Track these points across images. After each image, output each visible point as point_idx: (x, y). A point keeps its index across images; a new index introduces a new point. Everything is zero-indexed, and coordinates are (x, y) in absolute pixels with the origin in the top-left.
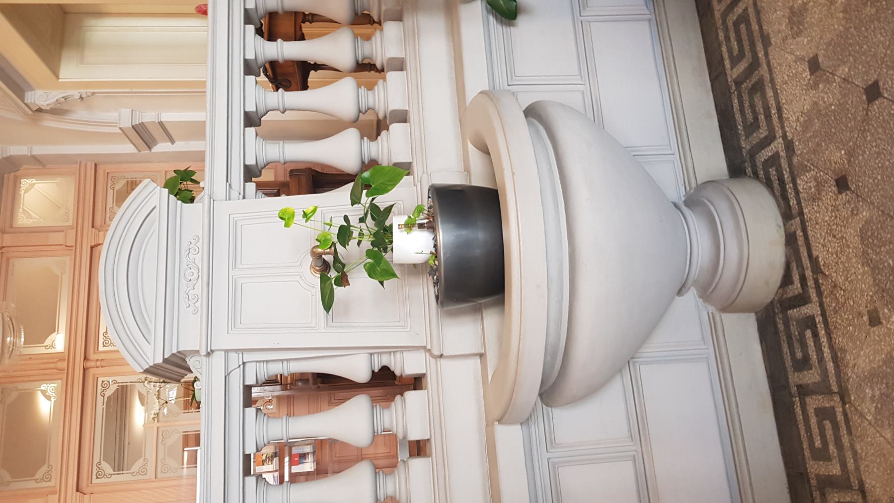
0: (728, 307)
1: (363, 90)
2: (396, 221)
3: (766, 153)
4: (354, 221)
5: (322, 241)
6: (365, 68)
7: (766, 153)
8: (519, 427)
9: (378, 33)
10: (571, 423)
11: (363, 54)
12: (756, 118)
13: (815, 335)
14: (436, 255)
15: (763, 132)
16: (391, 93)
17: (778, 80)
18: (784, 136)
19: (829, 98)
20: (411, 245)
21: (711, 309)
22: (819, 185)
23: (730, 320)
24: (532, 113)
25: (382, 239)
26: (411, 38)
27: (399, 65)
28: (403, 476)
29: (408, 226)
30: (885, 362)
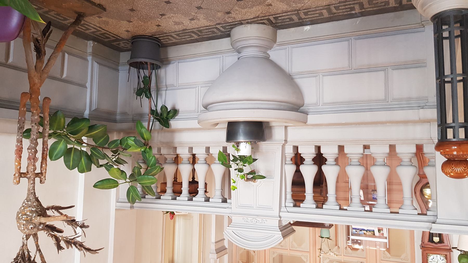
0: (274, 40)
1: (199, 162)
2: (237, 154)
3: (221, 29)
4: (237, 167)
5: (242, 177)
6: (194, 160)
7: (221, 29)
8: (308, 116)
9: (180, 156)
10: (310, 98)
11: (333, 162)
12: (210, 31)
13: (280, 17)
14: (247, 142)
15: (215, 30)
16: (200, 153)
17: (198, 27)
18: (215, 25)
19: (202, 16)
20: (245, 149)
21: (275, 45)
22: (229, 17)
23: (279, 40)
24: (206, 107)
25: (243, 159)
26: (182, 144)
27: (191, 149)
28: (351, 155)
29: (238, 150)
30: (283, 2)
